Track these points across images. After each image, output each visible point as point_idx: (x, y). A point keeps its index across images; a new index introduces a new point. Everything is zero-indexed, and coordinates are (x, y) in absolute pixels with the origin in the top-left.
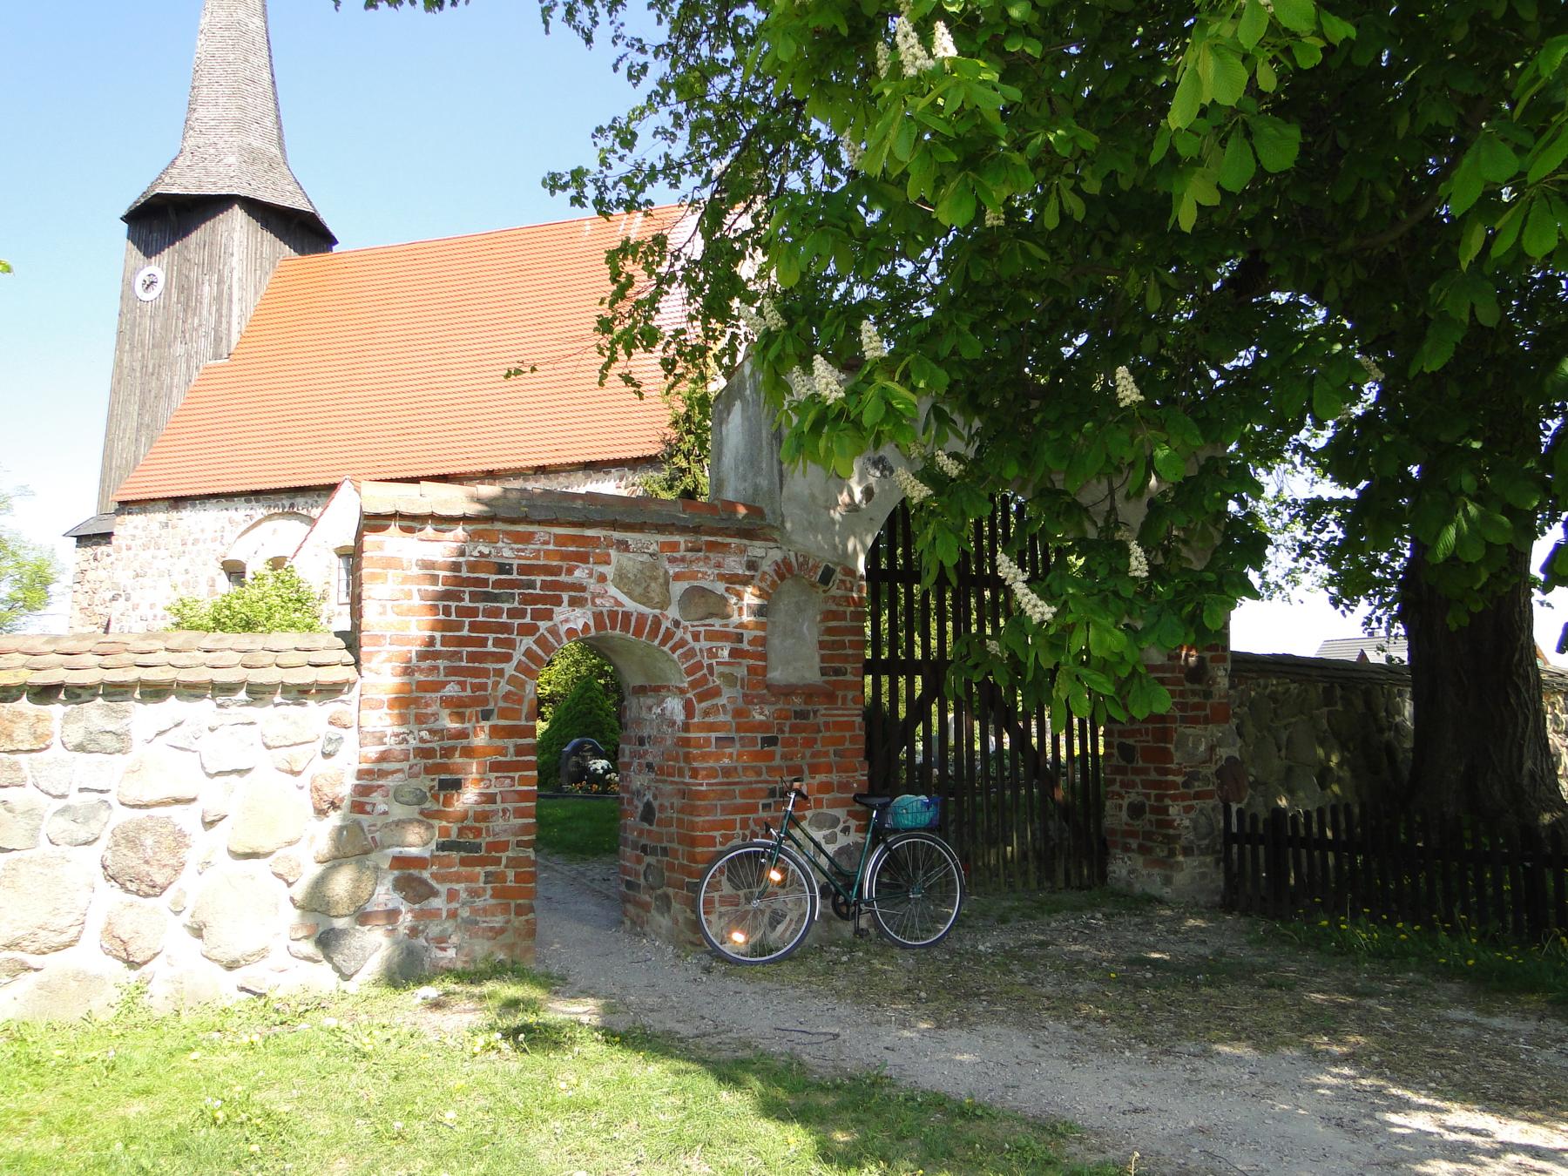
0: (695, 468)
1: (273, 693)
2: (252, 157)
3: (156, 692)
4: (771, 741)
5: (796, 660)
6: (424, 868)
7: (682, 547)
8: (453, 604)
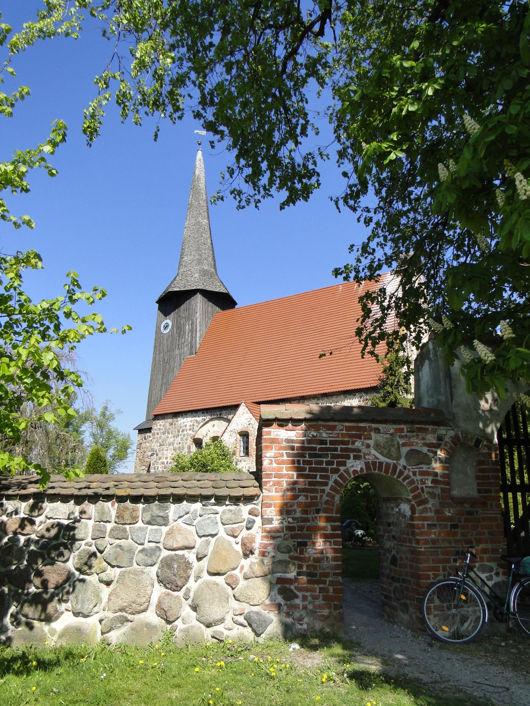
0: (395, 392)
1: (226, 500)
2: (204, 273)
3: (178, 499)
4: (455, 526)
5: (466, 487)
6: (292, 584)
7: (405, 430)
8: (302, 459)
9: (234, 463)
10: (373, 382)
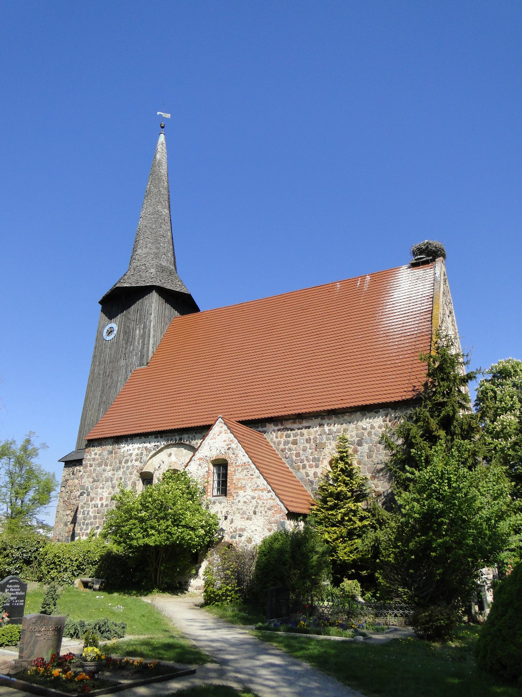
2: (162, 269)
9: (204, 508)
10: (404, 394)
